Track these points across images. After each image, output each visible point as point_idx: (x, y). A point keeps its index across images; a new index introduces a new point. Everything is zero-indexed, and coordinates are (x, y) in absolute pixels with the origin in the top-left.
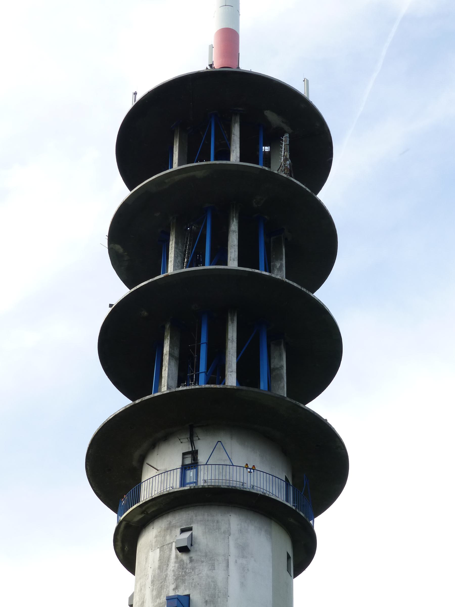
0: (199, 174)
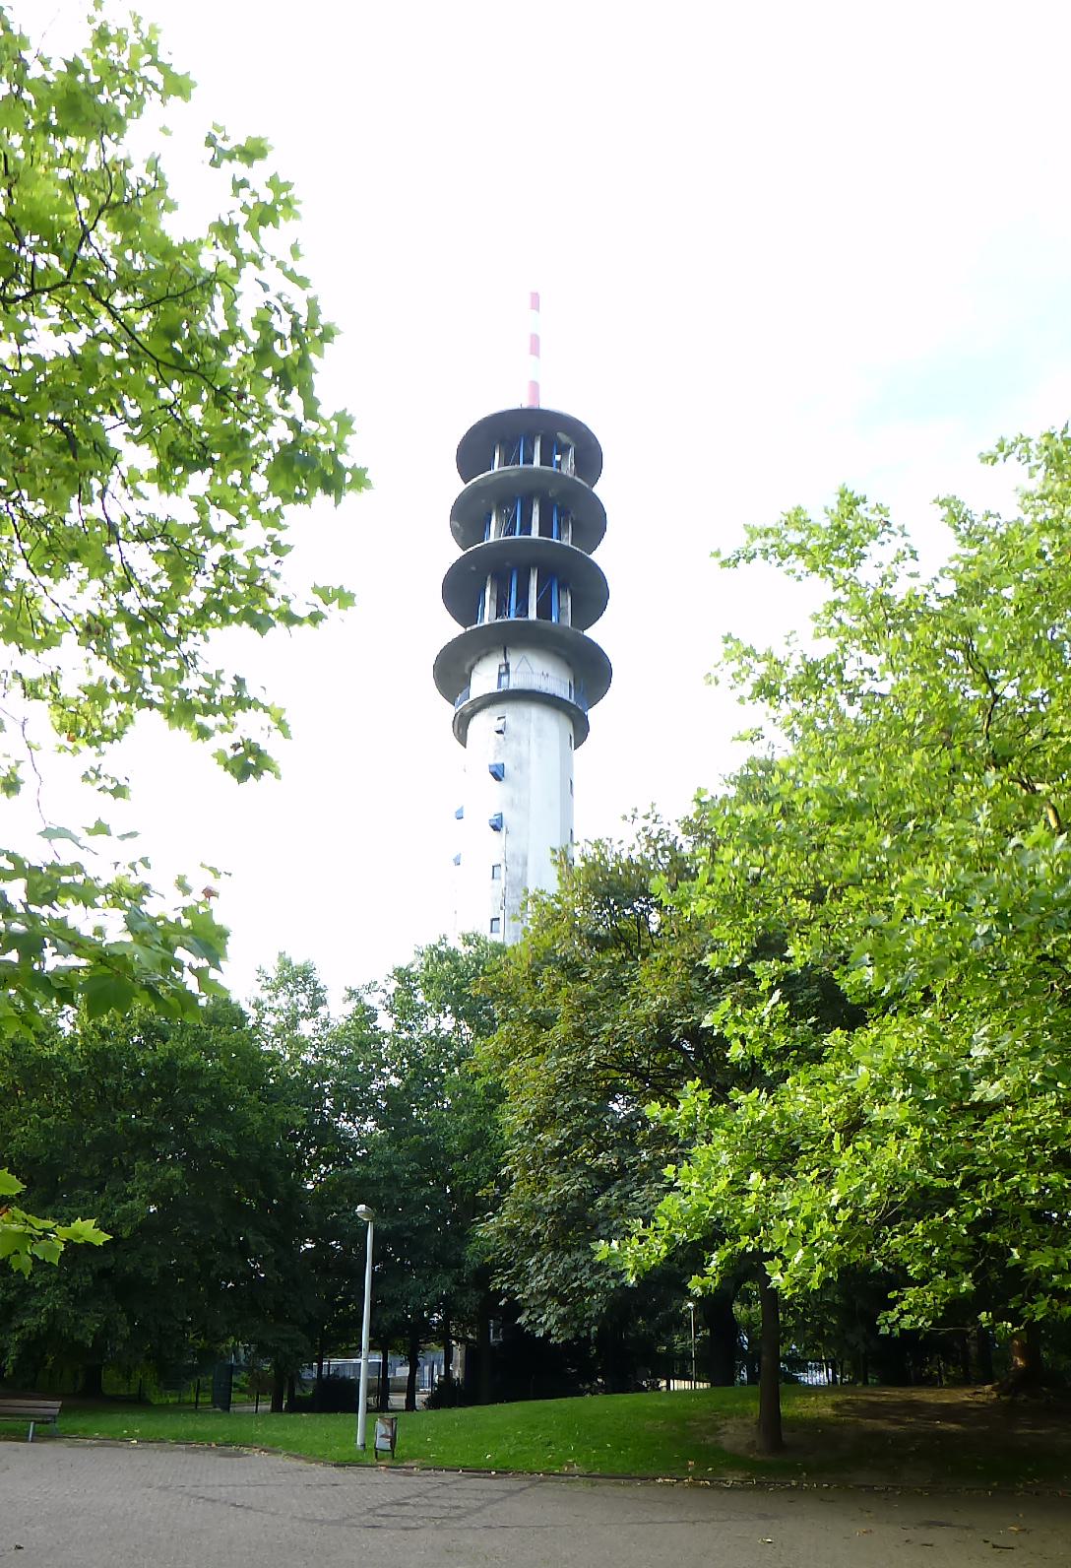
0: (513, 474)
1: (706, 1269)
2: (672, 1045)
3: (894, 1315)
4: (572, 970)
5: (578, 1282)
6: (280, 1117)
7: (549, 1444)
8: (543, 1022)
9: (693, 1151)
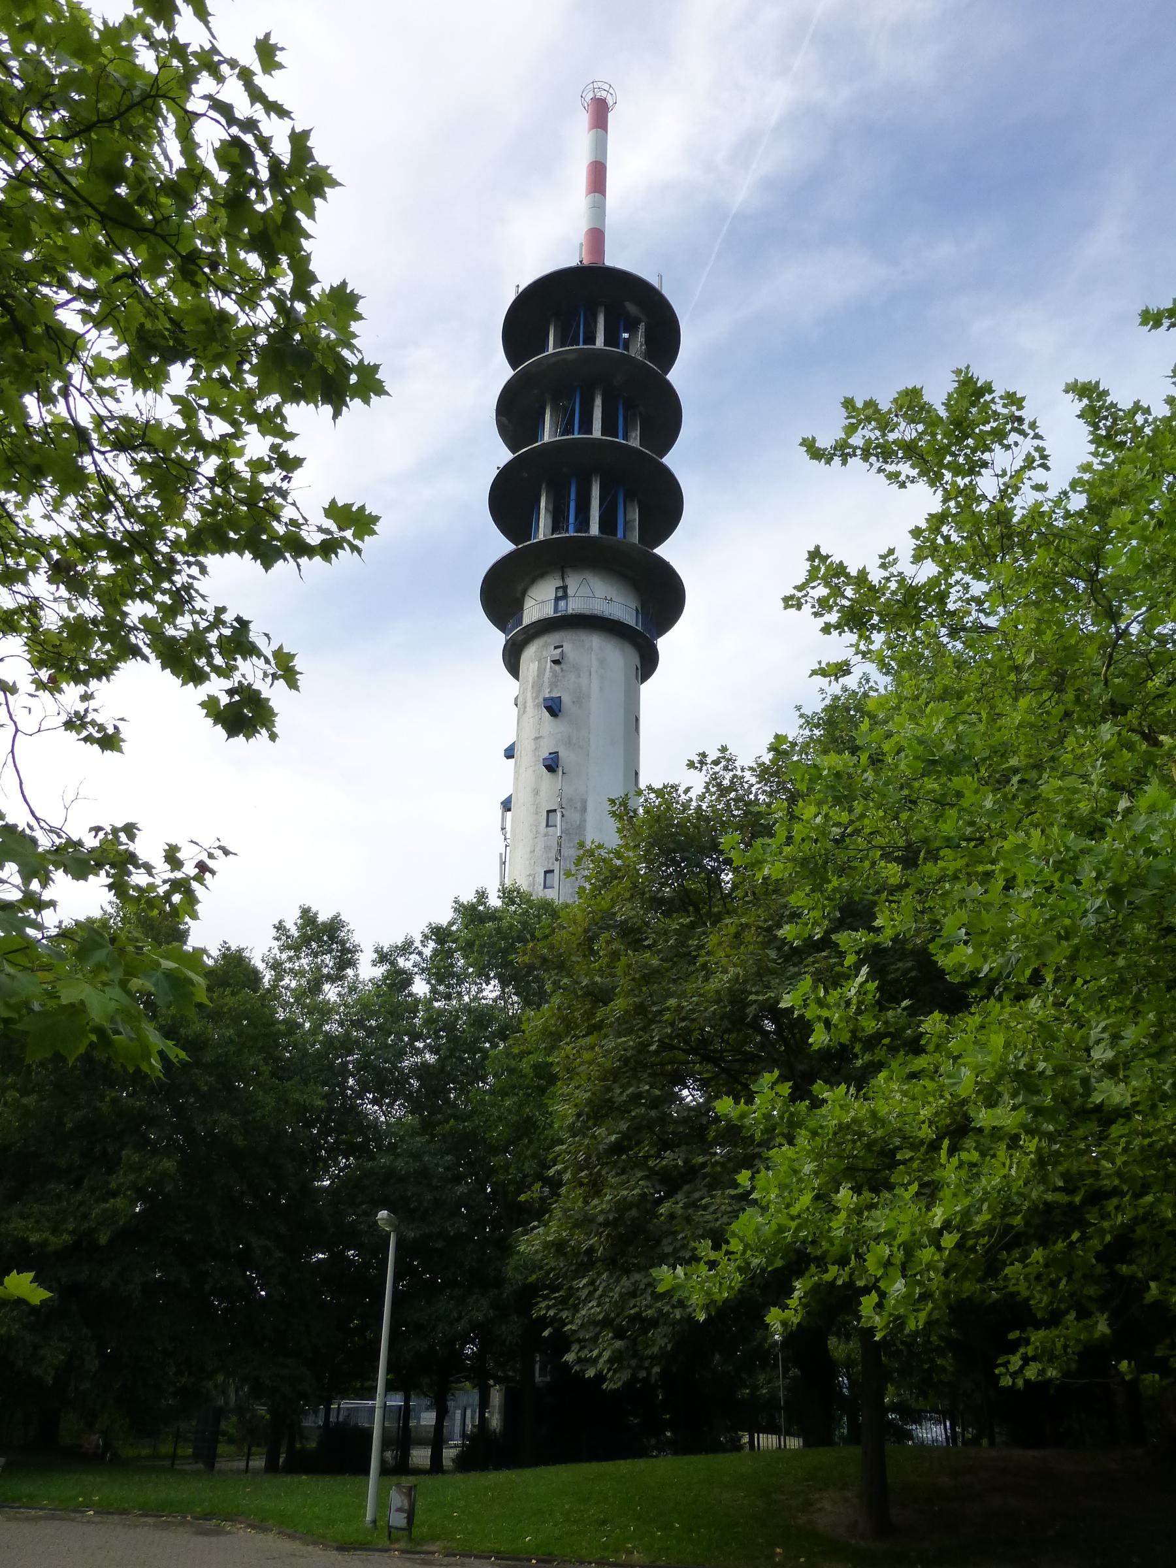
0: (570, 357)
1: (788, 1301)
2: (749, 1025)
3: (1016, 1361)
4: (632, 935)
5: (637, 1309)
6: (297, 1096)
7: (604, 1523)
8: (601, 996)
9: (772, 1153)
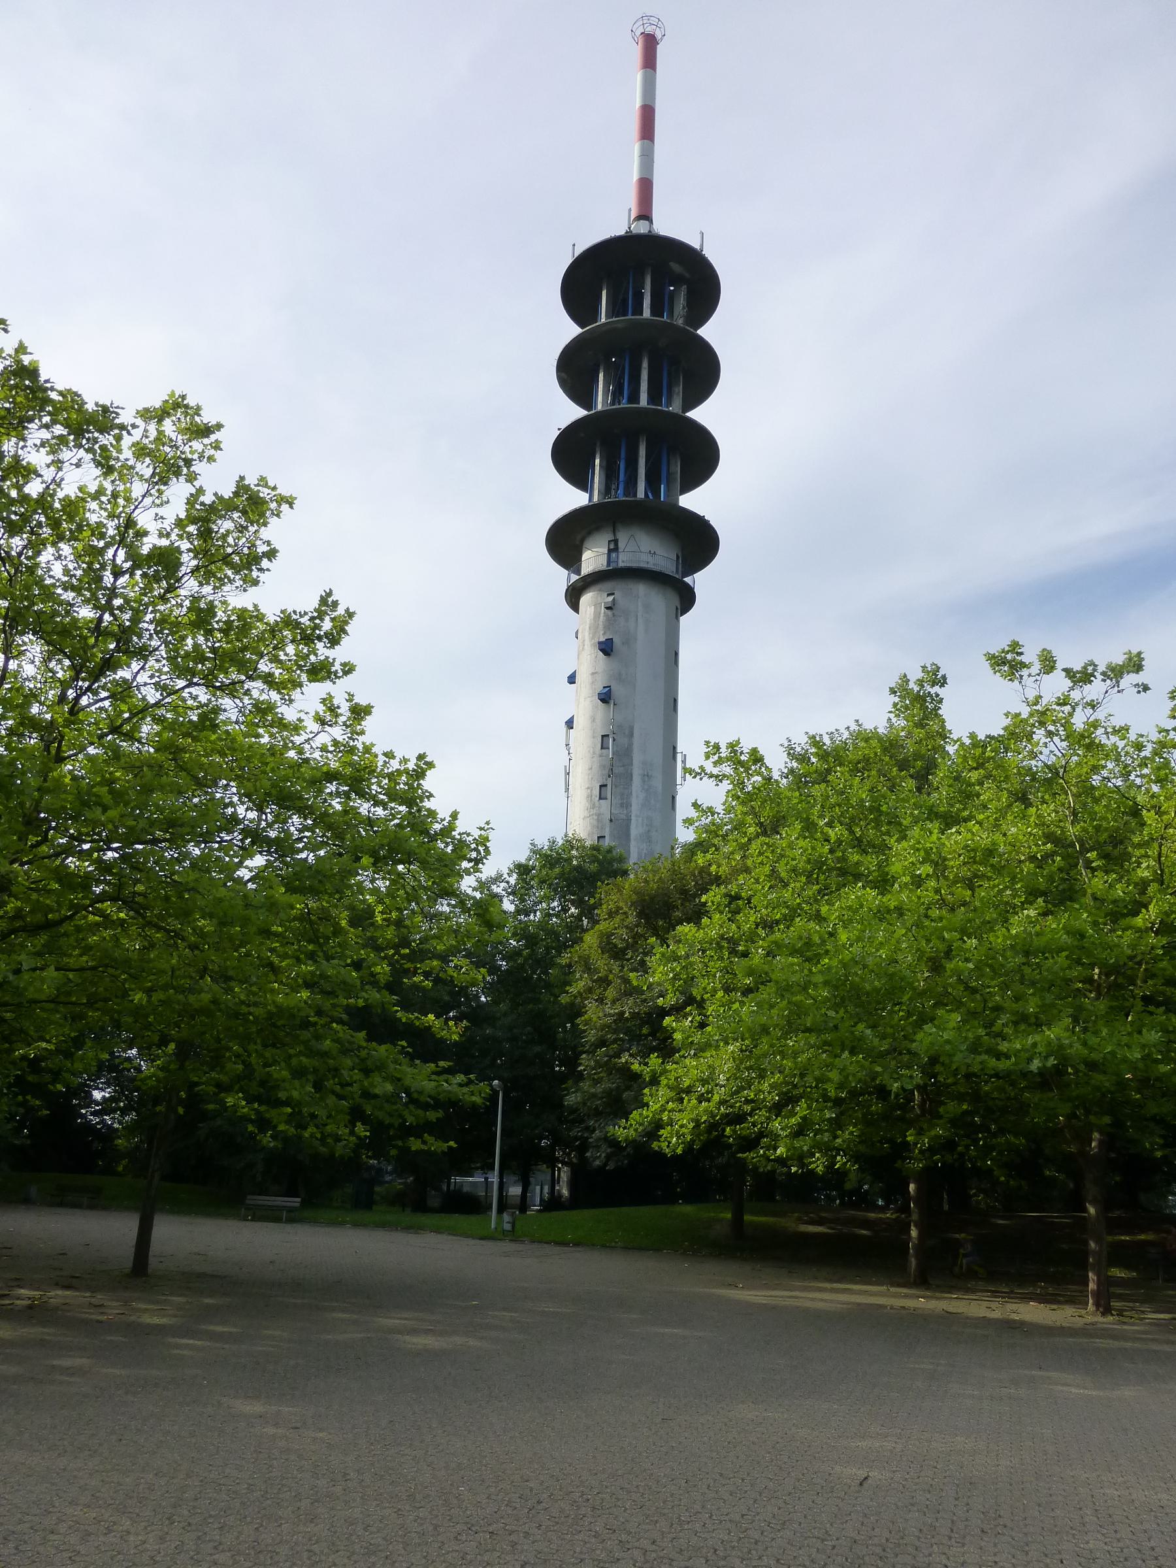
0: (619, 325)
